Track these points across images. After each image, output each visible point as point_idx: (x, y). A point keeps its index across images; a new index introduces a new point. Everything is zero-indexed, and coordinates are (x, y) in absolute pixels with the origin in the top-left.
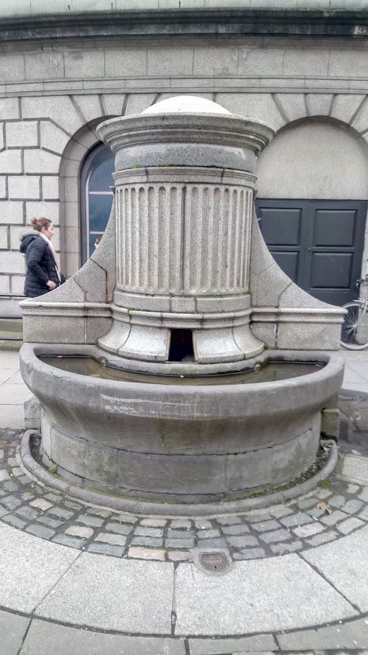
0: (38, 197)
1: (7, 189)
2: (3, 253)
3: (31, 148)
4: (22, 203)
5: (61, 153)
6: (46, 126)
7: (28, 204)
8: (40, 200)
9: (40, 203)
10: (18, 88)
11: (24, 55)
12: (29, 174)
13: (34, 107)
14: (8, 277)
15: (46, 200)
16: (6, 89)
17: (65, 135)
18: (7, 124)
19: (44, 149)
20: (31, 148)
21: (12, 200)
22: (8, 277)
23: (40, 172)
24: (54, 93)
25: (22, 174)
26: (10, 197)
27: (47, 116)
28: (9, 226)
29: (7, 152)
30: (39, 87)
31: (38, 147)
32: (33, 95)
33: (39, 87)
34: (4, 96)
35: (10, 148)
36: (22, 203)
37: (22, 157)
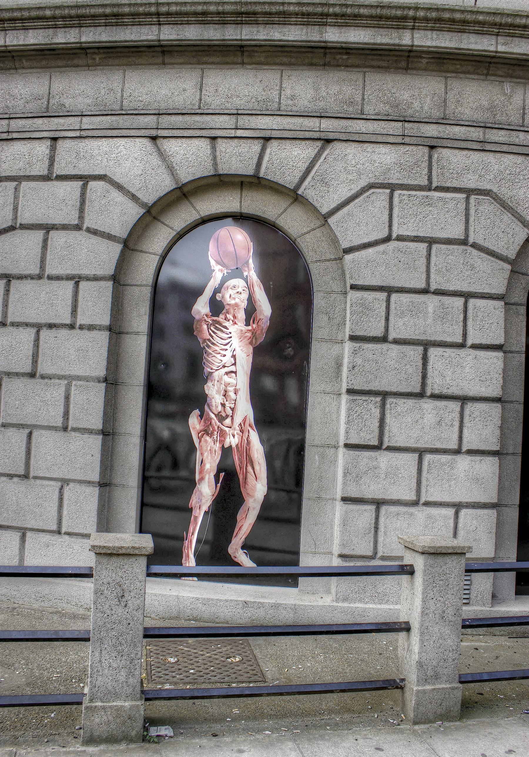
0: (459, 339)
1: (387, 319)
2: (474, 1)
3: (449, 242)
4: (420, 349)
5: (512, 254)
6: (484, 208)
7: (433, 352)
8: (462, 346)
9: (463, 352)
10: (431, 130)
11: (446, 78)
12: (439, 293)
13: (459, 166)
14: (373, 507)
15: (475, 347)
16: (404, 128)
17: (54, 432)
18: (397, 193)
19: (474, 246)
20: (449, 242)
21: (396, 342)
22: (373, 507)
23: (465, 288)
24: (505, 148)
25: (425, 291)
26: (392, 336)
27: (488, 187)
28: (384, 395)
29: (392, 245)
30: (476, 134)
31: (464, 242)
32: (462, 145)
33: (476, 134)
34: (399, 140)
35: (400, 238)
36: (420, 349)
37: (388, 301)
